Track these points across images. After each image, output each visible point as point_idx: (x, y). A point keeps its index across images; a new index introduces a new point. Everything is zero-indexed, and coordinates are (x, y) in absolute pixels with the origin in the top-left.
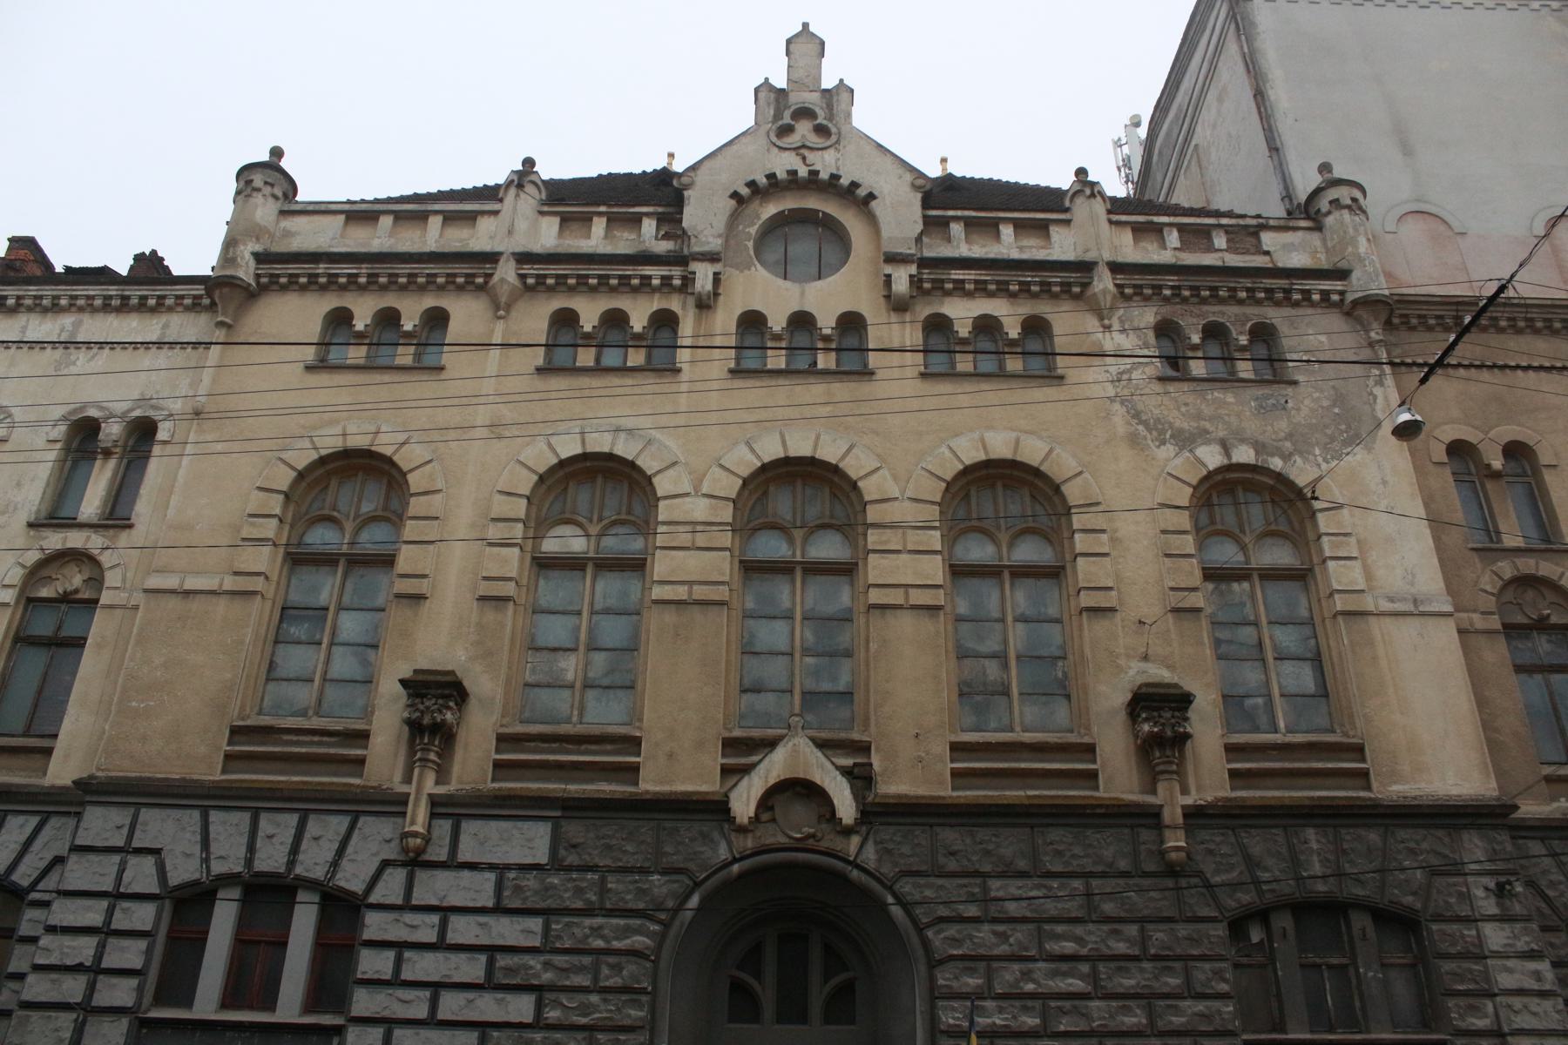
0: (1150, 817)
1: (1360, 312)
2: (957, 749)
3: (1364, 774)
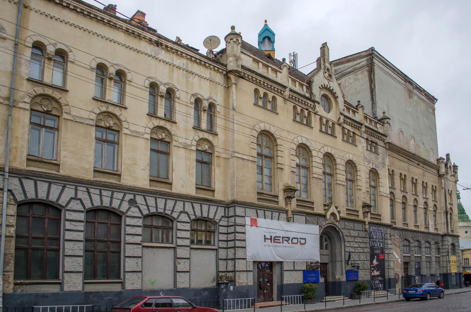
0: (364, 222)
1: (387, 144)
2: (347, 209)
3: (380, 219)
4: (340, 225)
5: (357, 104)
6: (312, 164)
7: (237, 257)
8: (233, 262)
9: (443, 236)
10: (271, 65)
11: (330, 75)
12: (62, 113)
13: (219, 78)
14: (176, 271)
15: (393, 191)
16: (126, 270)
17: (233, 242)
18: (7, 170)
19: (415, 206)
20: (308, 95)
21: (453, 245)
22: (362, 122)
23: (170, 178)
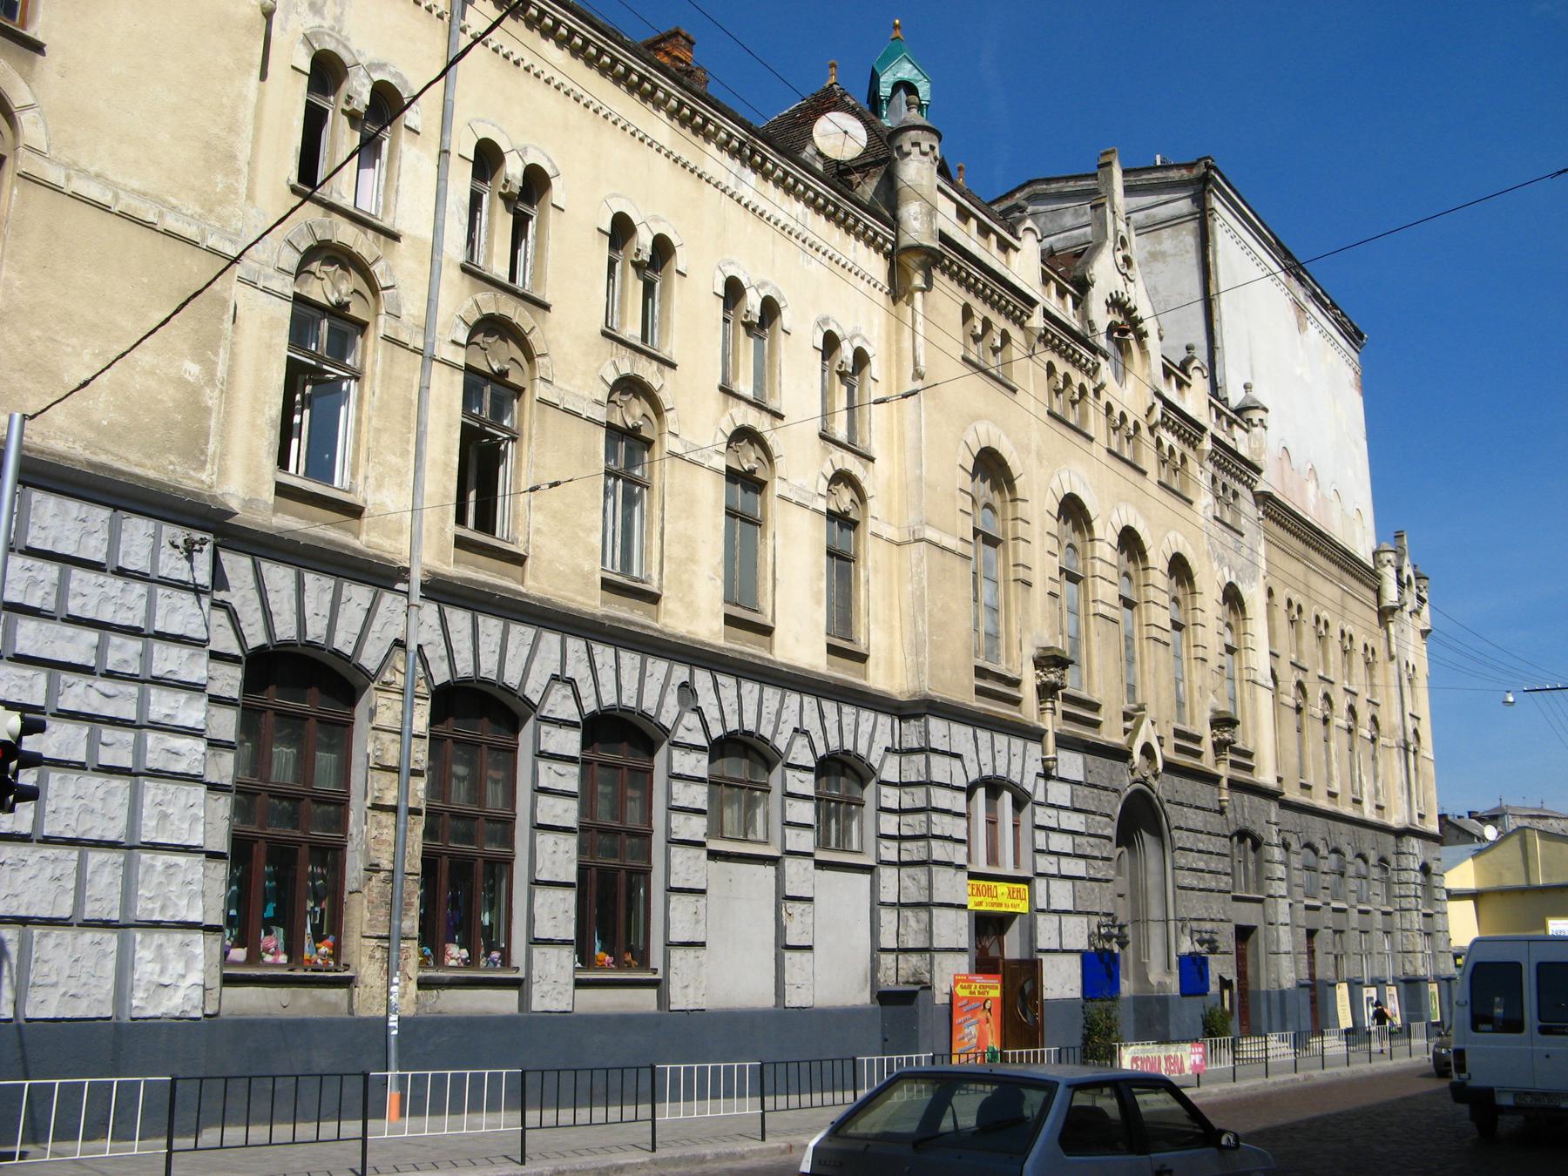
4: (1163, 788)
5: (1183, 355)
6: (1093, 565)
7: (936, 899)
8: (924, 915)
9: (1400, 834)
10: (996, 227)
11: (1127, 261)
12: (533, 379)
13: (876, 265)
14: (783, 947)
15: (648, 372)
16: (674, 938)
17: (922, 843)
18: (417, 577)
19: (746, 482)
20: (1076, 325)
21: (1425, 869)
22: (1203, 421)
23: (766, 604)
